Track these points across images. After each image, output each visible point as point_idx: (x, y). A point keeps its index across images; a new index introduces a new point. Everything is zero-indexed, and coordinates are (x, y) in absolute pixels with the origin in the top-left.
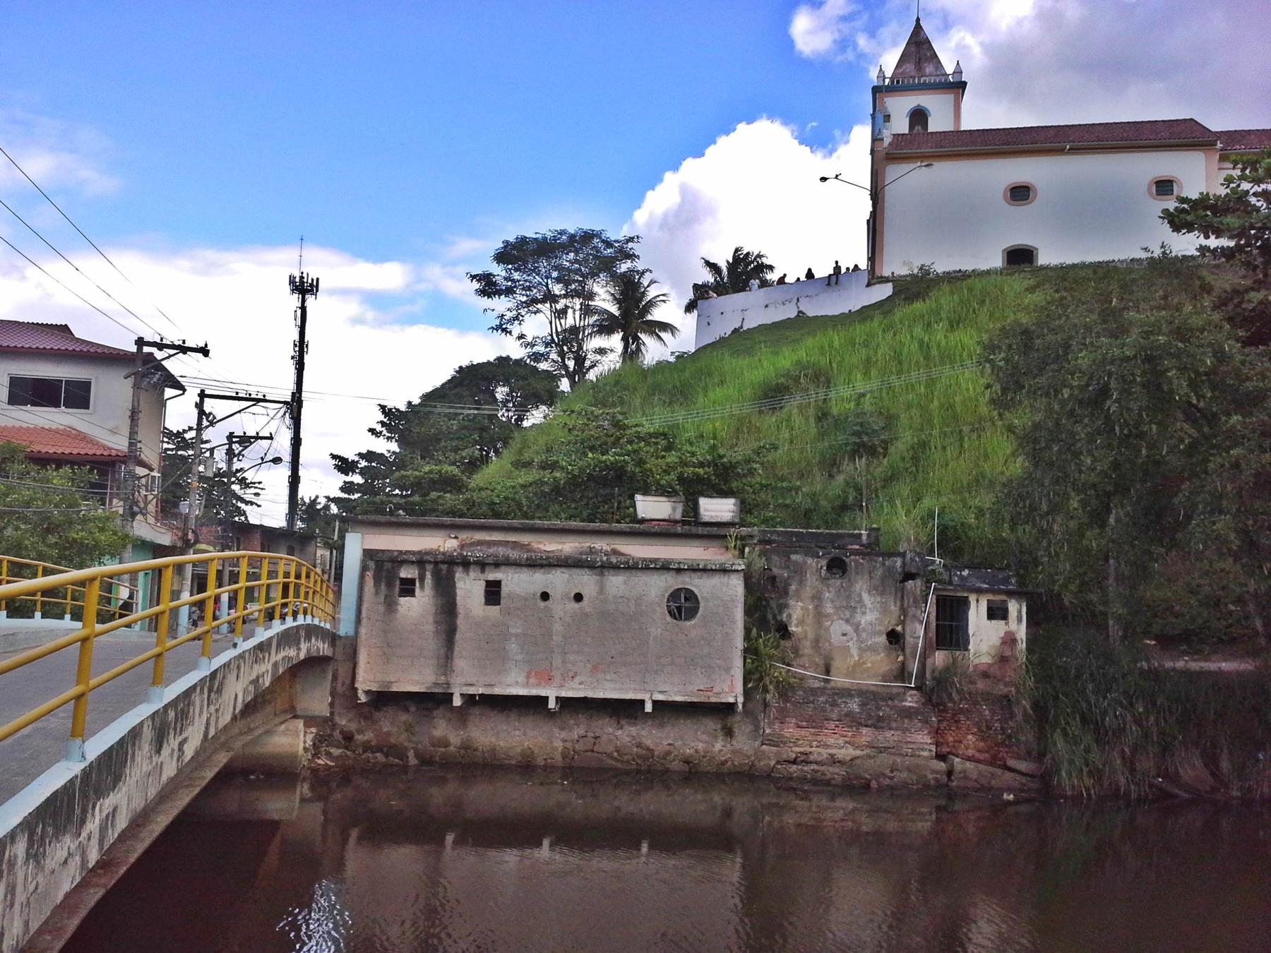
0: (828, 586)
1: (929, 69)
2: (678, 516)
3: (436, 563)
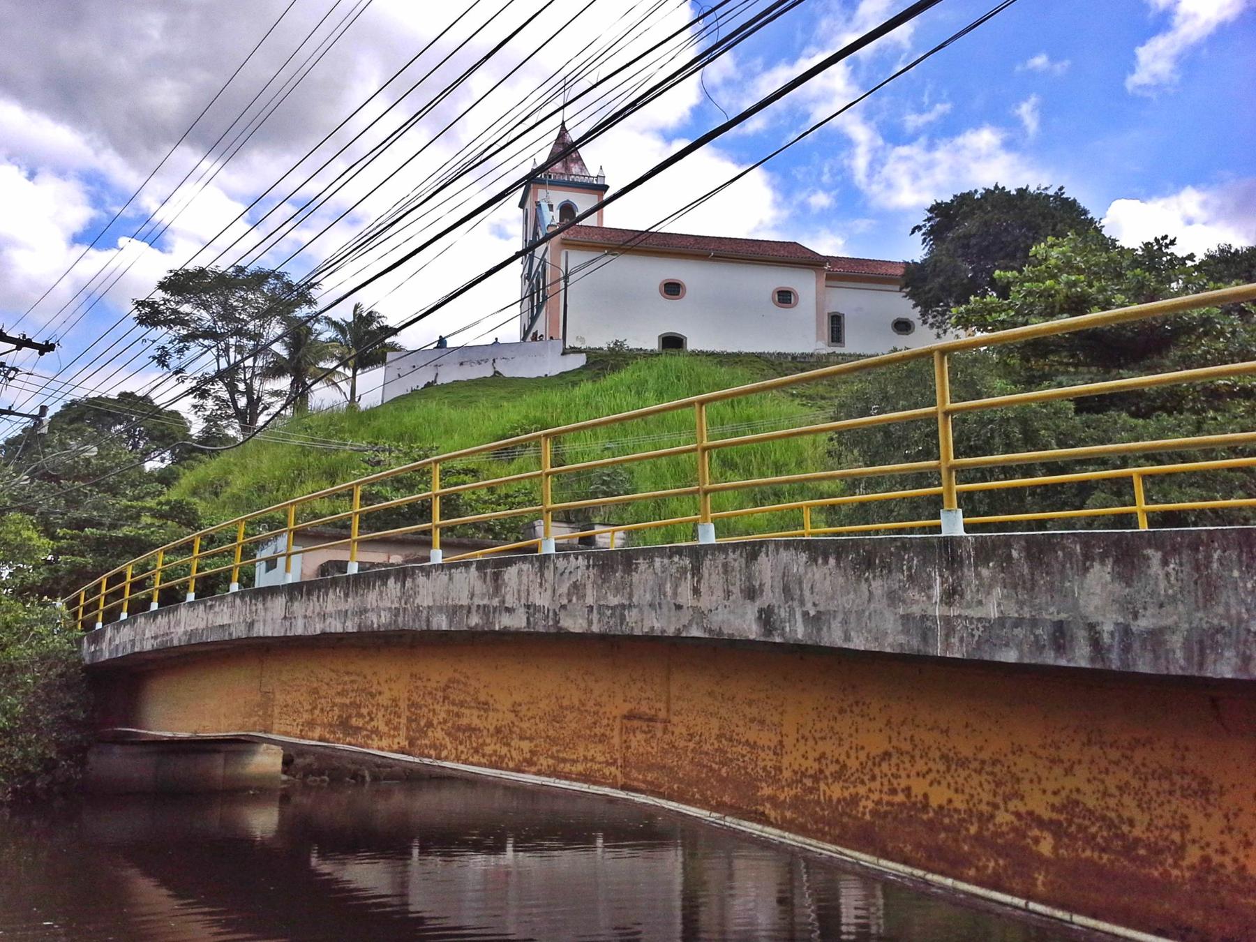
1: (575, 169)
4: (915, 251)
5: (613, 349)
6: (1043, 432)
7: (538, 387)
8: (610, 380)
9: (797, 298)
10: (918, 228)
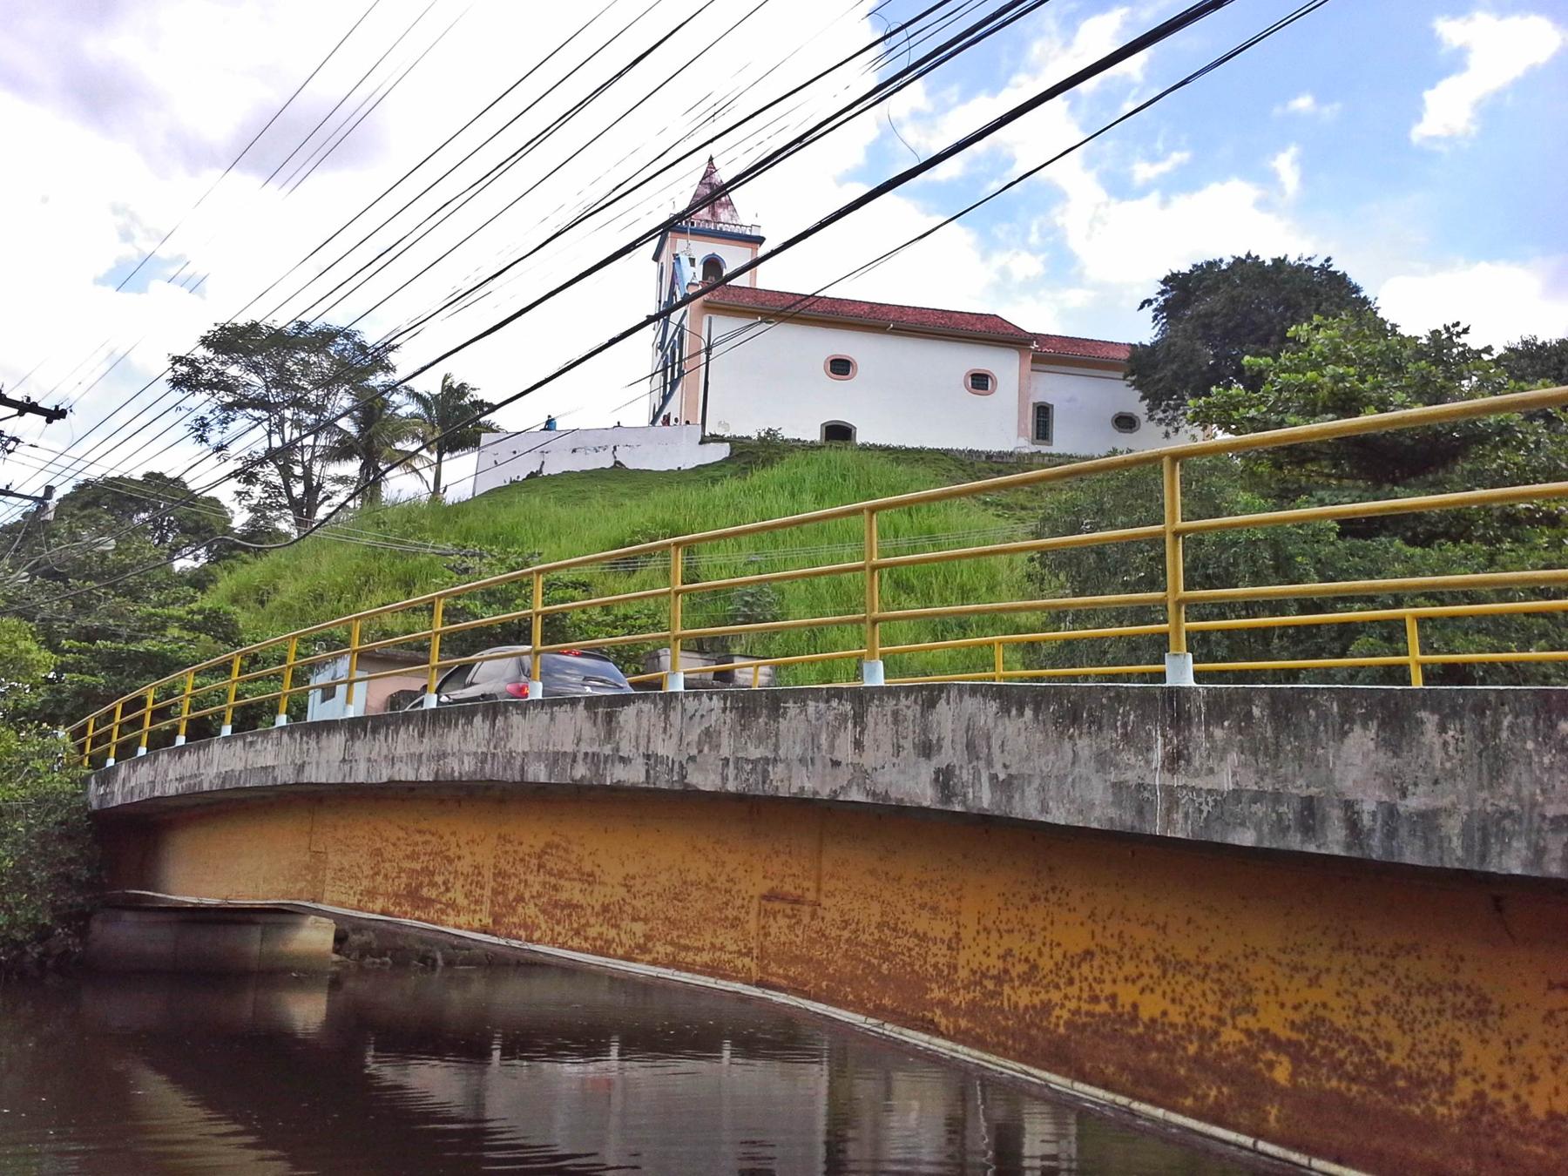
8: (758, 477)
9: (995, 383)
10: (1149, 302)
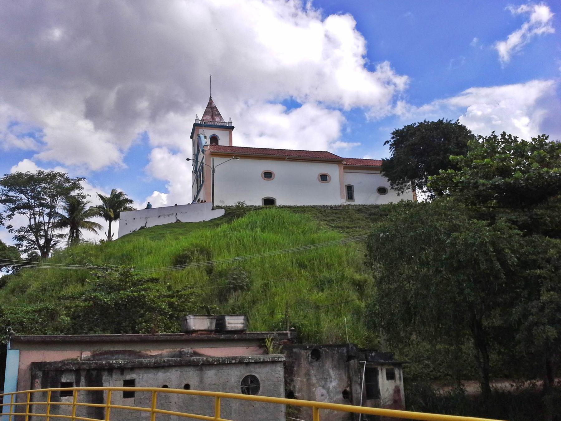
0: (313, 366)
1: (217, 119)
2: (213, 327)
3: (88, 371)
4: (387, 154)
5: (238, 206)
6: (507, 251)
7: (199, 228)
8: (235, 223)
9: (330, 178)
10: (388, 142)
